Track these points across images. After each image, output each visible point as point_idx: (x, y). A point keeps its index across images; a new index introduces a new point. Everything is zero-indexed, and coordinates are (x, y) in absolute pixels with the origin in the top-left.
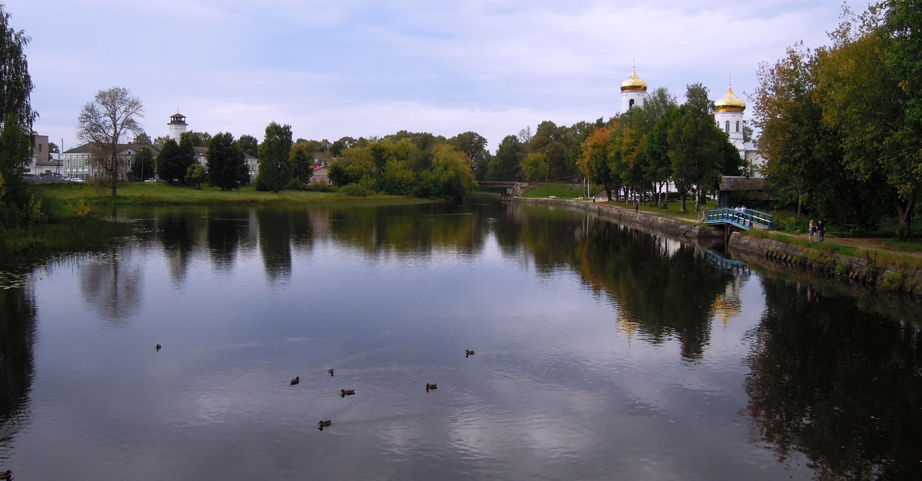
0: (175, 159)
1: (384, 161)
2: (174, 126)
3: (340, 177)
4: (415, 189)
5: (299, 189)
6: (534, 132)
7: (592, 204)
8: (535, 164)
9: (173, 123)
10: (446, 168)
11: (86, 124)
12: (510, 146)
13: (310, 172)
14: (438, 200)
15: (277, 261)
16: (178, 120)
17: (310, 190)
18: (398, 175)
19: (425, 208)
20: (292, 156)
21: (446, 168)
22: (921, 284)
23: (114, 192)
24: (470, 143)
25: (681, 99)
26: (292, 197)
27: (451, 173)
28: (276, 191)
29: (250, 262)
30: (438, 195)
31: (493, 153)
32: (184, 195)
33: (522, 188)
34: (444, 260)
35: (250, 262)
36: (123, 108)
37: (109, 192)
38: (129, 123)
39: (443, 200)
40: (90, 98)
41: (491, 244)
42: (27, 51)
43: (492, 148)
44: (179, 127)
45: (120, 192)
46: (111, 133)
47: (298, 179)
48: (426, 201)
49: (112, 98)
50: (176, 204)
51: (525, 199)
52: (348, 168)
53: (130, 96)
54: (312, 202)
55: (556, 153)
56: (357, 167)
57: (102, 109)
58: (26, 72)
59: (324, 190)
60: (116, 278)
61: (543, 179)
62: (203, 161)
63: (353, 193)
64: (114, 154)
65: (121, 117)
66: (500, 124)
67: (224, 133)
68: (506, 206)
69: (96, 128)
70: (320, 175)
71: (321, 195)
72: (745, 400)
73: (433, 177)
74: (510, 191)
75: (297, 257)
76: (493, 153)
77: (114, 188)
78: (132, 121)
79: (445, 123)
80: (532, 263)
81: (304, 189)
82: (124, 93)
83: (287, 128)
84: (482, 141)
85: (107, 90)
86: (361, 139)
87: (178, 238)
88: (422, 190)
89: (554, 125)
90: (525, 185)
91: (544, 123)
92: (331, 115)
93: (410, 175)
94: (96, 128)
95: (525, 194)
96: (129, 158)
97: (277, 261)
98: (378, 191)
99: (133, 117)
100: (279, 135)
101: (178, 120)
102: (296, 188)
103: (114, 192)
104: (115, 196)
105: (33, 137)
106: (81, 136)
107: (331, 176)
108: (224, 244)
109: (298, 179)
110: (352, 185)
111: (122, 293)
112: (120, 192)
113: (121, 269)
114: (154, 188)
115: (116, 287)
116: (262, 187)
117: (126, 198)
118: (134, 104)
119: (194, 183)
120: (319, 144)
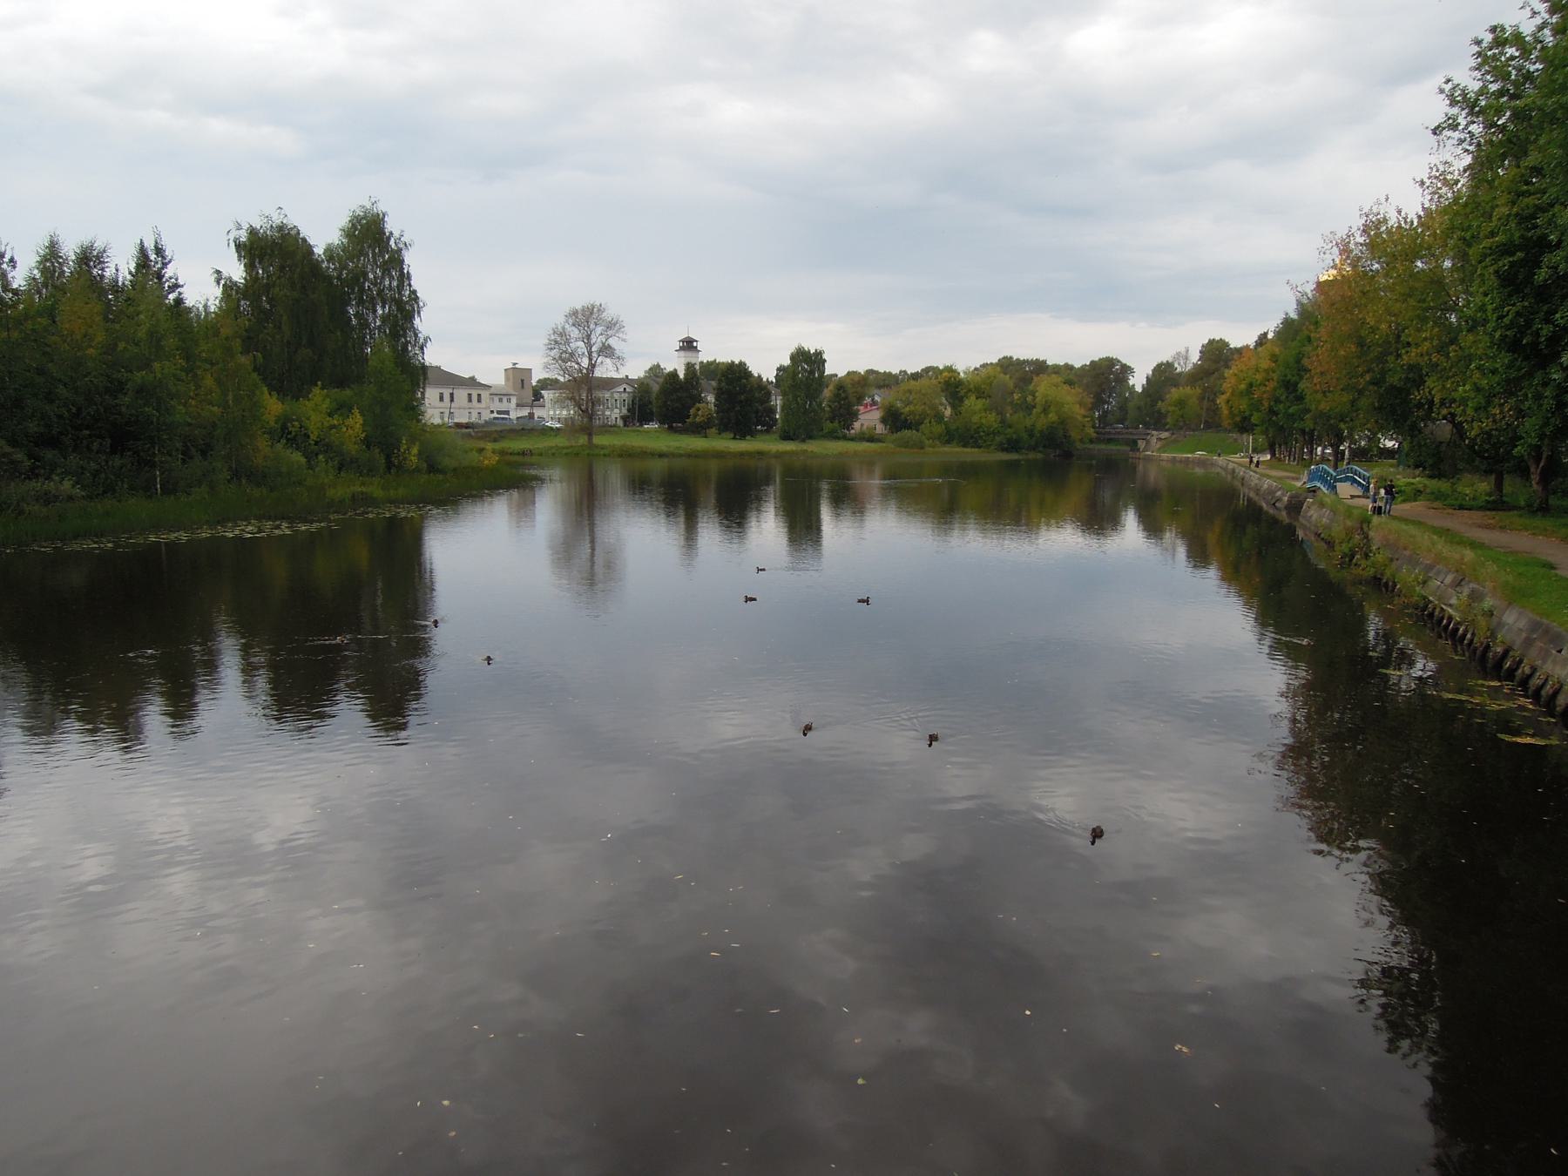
0: (668, 400)
1: (961, 400)
2: (682, 353)
3: (894, 420)
4: (998, 439)
5: (838, 438)
6: (1195, 357)
7: (1259, 473)
8: (1181, 403)
9: (682, 349)
10: (1045, 410)
11: (553, 353)
12: (1164, 375)
13: (854, 416)
14: (1031, 456)
16: (689, 345)
17: (852, 439)
18: (975, 419)
19: (1012, 466)
20: (827, 393)
21: (1045, 410)
22: (1567, 670)
24: (1105, 376)
25: (120, 265)
26: (823, 449)
27: (1052, 417)
28: (803, 441)
29: (767, 529)
30: (1034, 448)
31: (1139, 389)
32: (677, 444)
33: (1159, 439)
34: (1062, 541)
35: (767, 529)
36: (599, 329)
38: (606, 350)
39: (1040, 456)
40: (559, 320)
41: (1130, 520)
42: (411, 260)
43: (1138, 381)
44: (689, 354)
45: (597, 440)
46: (585, 363)
47: (836, 424)
48: (1014, 456)
49: (586, 318)
51: (1160, 455)
53: (609, 314)
54: (856, 453)
55: (1210, 393)
56: (920, 408)
59: (871, 439)
60: (593, 549)
62: (711, 398)
63: (906, 445)
64: (590, 390)
66: (1147, 346)
68: (1134, 468)
69: (567, 357)
70: (869, 418)
71: (865, 446)
72: (1297, 826)
73: (1028, 422)
74: (1141, 444)
75: (833, 528)
76: (1139, 389)
77: (590, 435)
79: (1068, 342)
80: (1181, 551)
81: (845, 438)
83: (819, 354)
84: (1126, 370)
85: (579, 307)
87: (678, 494)
88: (1009, 441)
89: (1227, 344)
90: (1165, 435)
91: (1211, 342)
92: (867, 338)
93: (992, 419)
94: (567, 357)
95: (1162, 449)
96: (625, 396)
98: (948, 442)
99: (612, 342)
100: (807, 364)
101: (689, 345)
102: (833, 436)
103: (590, 439)
104: (591, 445)
105: (424, 368)
106: (546, 367)
107: (884, 420)
108: (735, 508)
109: (836, 424)
110: (907, 433)
111: (599, 569)
112: (597, 440)
113: (598, 541)
114: (653, 437)
115: (593, 563)
116: (786, 437)
117: (603, 448)
119: (700, 429)
120: (895, 376)
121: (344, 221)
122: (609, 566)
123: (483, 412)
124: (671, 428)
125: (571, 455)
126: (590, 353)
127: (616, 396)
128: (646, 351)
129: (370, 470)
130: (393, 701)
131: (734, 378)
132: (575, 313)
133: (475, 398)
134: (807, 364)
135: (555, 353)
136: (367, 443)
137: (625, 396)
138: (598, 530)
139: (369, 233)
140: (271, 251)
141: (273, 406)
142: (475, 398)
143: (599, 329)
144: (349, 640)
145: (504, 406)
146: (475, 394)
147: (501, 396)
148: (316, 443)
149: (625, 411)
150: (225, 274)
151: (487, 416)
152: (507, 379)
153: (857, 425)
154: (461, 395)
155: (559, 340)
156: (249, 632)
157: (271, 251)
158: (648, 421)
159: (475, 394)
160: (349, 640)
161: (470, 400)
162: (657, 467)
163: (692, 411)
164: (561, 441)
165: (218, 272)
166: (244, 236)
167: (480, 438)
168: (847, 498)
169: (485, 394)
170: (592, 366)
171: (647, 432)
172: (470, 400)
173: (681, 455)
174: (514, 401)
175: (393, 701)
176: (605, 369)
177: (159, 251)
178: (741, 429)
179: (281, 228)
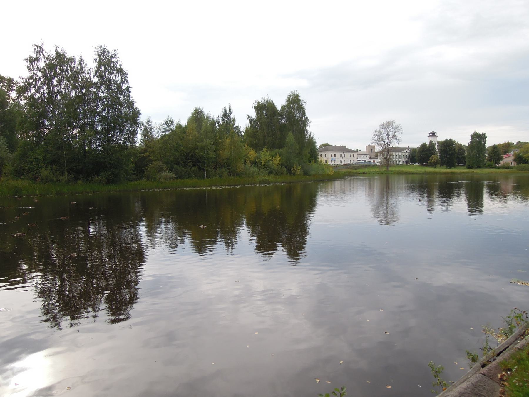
0: (422, 155)
3: (519, 159)
5: (492, 168)
9: (430, 136)
13: (501, 159)
15: (475, 205)
16: (433, 134)
17: (499, 168)
23: (387, 168)
27: (329, 192)
28: (476, 168)
29: (460, 204)
32: (421, 170)
35: (460, 204)
37: (385, 169)
38: (394, 137)
45: (390, 169)
47: (492, 162)
49: (387, 126)
50: (417, 174)
52: (526, 156)
53: (397, 123)
57: (383, 131)
58: (129, 96)
59: (508, 168)
61: (123, 73)
65: (391, 134)
67: (448, 139)
70: (508, 159)
71: (507, 170)
78: (396, 136)
81: (496, 167)
82: (393, 122)
83: (483, 134)
86: (10, 78)
87: (424, 188)
96: (407, 154)
97: (475, 205)
100: (478, 140)
102: (490, 166)
103: (387, 168)
104: (388, 170)
107: (515, 160)
110: (523, 165)
112: (390, 169)
113: (390, 203)
114: (416, 168)
116: (469, 167)
117: (392, 171)
118: (396, 128)
119: (434, 165)
121: (286, 97)
122: (393, 213)
123: (355, 160)
124: (422, 165)
125: (381, 174)
126: (388, 138)
127: (403, 154)
128: (412, 139)
129: (281, 174)
130: (295, 251)
131: (448, 146)
132: (384, 124)
133: (352, 155)
134: (478, 140)
135: (376, 139)
136: (282, 165)
137: (407, 154)
138: (390, 200)
139: (295, 102)
140: (265, 109)
141: (253, 154)
142: (352, 155)
143: (392, 130)
144: (282, 228)
145: (365, 158)
146: (352, 154)
147: (364, 155)
148: (264, 165)
149: (406, 159)
150: (250, 116)
151: (356, 161)
152: (367, 149)
153: (502, 163)
154: (348, 154)
155: (378, 134)
156: (252, 225)
157: (265, 109)
158: (415, 163)
159: (352, 154)
160: (282, 228)
161: (351, 156)
162: (417, 177)
163: (430, 158)
164: (377, 170)
165: (248, 116)
166: (256, 104)
167: (351, 169)
168: (495, 190)
169: (356, 154)
170: (389, 142)
171: (416, 166)
172: (351, 156)
173: (420, 174)
174: (368, 156)
175: (295, 251)
176: (394, 144)
177: (230, 111)
178: (450, 165)
179: (267, 101)
